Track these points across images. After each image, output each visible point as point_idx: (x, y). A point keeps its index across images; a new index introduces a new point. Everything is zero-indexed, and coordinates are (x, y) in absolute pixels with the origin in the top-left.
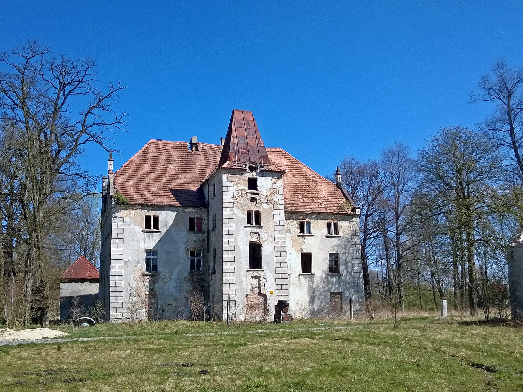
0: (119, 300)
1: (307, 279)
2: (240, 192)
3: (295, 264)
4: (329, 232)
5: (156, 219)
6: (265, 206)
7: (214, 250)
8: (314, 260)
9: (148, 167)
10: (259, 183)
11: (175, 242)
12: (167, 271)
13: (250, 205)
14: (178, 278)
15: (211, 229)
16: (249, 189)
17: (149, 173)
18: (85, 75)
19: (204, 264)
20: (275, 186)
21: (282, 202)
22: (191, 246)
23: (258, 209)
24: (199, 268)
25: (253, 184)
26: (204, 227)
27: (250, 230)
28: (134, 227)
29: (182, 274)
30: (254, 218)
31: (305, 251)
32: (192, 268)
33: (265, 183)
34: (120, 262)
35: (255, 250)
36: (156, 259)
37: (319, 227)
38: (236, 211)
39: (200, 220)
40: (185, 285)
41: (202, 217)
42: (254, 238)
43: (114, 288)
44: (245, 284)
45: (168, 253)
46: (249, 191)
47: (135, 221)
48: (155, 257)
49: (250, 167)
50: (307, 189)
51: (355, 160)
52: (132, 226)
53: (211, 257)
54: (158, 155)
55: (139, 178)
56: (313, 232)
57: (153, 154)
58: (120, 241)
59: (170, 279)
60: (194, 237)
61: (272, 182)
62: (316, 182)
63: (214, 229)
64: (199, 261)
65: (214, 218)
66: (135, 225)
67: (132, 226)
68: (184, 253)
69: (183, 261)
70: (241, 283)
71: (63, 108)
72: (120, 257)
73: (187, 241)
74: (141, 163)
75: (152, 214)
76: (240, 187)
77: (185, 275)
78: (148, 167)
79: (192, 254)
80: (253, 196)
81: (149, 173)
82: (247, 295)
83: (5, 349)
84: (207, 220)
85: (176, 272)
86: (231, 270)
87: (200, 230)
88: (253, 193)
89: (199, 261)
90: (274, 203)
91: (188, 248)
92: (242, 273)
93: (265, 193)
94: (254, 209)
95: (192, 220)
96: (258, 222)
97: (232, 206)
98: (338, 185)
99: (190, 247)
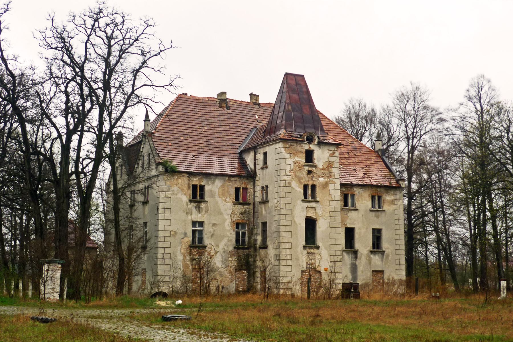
0: (288, 229)
1: (350, 256)
2: (297, 164)
4: (373, 206)
6: (321, 179)
7: (265, 224)
8: (357, 236)
9: (183, 129)
10: (315, 155)
11: (221, 214)
12: (213, 244)
13: (307, 178)
14: (224, 252)
15: (258, 199)
16: (306, 162)
18: (142, 33)
19: (250, 238)
20: (332, 159)
22: (236, 218)
23: (315, 183)
24: (243, 241)
25: (309, 155)
27: (306, 204)
28: (181, 197)
29: (228, 247)
31: (349, 226)
32: (237, 241)
33: (321, 156)
34: (168, 234)
35: (311, 224)
36: (202, 231)
37: (363, 201)
38: (294, 184)
40: (230, 259)
41: (248, 187)
42: (311, 214)
43: (161, 261)
44: (301, 260)
45: (214, 225)
46: (306, 164)
47: (182, 190)
48: (201, 229)
49: (307, 139)
50: (347, 156)
52: (179, 195)
56: (358, 205)
58: (168, 211)
59: (216, 252)
60: (240, 209)
61: (328, 155)
64: (244, 234)
66: (182, 195)
67: (179, 195)
68: (230, 225)
69: (228, 234)
70: (297, 259)
71: (119, 68)
72: (168, 228)
73: (233, 213)
75: (195, 181)
76: (298, 159)
77: (231, 248)
79: (237, 225)
80: (310, 169)
82: (302, 271)
84: (252, 191)
85: (222, 246)
86: (288, 246)
87: (245, 203)
88: (310, 166)
90: (330, 177)
91: (234, 220)
92: (299, 250)
93: (321, 167)
94: (310, 183)
95: (237, 190)
96: (313, 196)
97: (289, 179)
99: (235, 218)
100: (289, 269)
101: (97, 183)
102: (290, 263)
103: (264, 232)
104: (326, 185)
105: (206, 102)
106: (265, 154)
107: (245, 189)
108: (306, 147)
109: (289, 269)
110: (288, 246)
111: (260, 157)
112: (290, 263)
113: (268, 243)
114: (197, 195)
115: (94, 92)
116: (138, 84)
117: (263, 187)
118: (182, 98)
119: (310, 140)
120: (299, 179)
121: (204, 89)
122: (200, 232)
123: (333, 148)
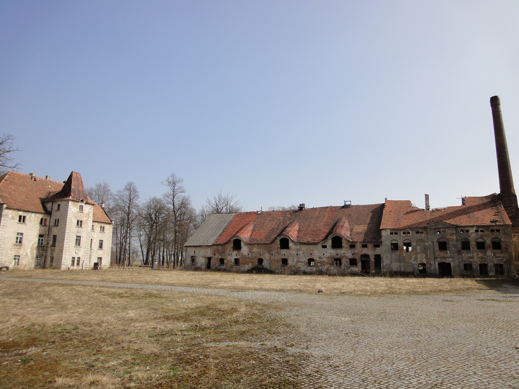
3: (96, 244)
4: (101, 231)
7: (55, 237)
17: (14, 191)
20: (90, 210)
21: (92, 218)
24: (42, 243)
25: (81, 208)
26: (48, 224)
30: (79, 223)
32: (39, 243)
39: (46, 219)
51: (7, 155)
54: (16, 180)
58: (5, 227)
60: (43, 228)
64: (42, 240)
83: (518, 293)
85: (31, 245)
86: (67, 246)
87: (45, 225)
89: (42, 240)
96: (81, 225)
100: (67, 256)
101: (172, 264)
102: (67, 253)
104: (87, 220)
106: (59, 205)
107: (46, 219)
108: (80, 204)
109: (67, 256)
111: (55, 206)
112: (67, 253)
113: (56, 244)
117: (56, 220)
119: (82, 201)
120: (76, 217)
123: (91, 206)
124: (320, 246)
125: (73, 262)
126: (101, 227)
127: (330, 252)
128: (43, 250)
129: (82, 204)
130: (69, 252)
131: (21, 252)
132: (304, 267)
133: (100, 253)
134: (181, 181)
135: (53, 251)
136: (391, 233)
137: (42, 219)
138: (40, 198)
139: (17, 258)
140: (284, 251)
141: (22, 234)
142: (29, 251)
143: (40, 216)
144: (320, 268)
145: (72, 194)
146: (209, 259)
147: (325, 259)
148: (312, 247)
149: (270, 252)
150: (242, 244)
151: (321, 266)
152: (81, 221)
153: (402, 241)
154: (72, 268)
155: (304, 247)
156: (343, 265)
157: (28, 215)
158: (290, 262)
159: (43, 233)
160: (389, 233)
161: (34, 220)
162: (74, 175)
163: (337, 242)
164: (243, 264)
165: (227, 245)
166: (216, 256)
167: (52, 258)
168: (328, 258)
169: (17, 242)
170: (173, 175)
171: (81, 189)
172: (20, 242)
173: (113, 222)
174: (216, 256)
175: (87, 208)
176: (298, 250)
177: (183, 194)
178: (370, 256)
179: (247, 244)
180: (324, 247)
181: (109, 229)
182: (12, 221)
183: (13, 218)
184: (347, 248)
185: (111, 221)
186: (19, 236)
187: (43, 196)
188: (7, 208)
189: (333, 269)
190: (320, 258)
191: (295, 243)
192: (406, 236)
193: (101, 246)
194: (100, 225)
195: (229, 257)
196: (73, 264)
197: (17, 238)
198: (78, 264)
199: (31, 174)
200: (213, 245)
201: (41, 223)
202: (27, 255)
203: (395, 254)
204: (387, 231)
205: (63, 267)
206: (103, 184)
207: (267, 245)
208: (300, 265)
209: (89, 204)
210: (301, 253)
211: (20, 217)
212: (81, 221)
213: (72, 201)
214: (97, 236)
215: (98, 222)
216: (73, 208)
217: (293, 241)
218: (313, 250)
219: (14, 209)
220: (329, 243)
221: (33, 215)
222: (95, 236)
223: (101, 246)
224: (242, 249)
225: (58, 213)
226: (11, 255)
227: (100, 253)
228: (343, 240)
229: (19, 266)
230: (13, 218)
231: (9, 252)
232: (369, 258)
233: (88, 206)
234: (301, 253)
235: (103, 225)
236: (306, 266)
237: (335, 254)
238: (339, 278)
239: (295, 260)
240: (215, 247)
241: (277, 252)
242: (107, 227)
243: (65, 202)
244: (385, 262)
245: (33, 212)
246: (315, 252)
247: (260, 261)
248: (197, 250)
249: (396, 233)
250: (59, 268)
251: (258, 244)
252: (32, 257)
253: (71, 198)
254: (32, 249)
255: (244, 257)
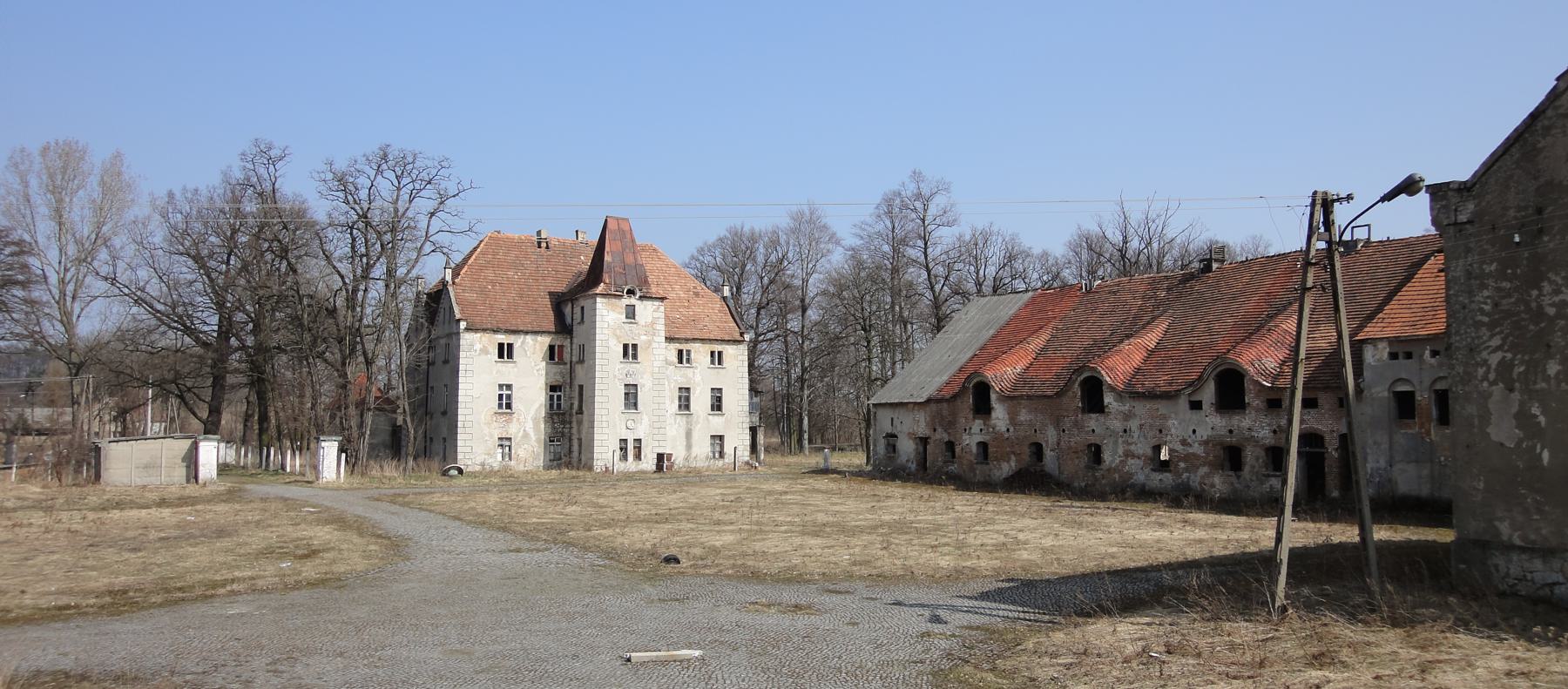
3: (701, 401)
5: (510, 346)
7: (581, 387)
17: (493, 283)
20: (656, 315)
24: (559, 406)
25: (631, 313)
26: (567, 357)
30: (630, 352)
32: (551, 406)
53: (576, 394)
55: (483, 291)
57: (495, 254)
60: (555, 369)
62: (697, 294)
63: (581, 361)
64: (559, 398)
65: (582, 348)
74: (482, 268)
78: (490, 274)
81: (493, 283)
86: (604, 412)
87: (561, 362)
89: (559, 398)
96: (635, 356)
98: (724, 299)
103: (581, 394)
104: (650, 343)
105: (519, 244)
107: (561, 347)
108: (626, 301)
110: (604, 412)
111: (577, 310)
114: (505, 352)
115: (380, 235)
116: (432, 230)
118: (183, 460)
119: (631, 292)
120: (618, 338)
121: (520, 230)
122: (509, 397)
124: (1183, 403)
125: (624, 449)
126: (712, 353)
127: (1212, 423)
128: (563, 422)
129: (633, 301)
130: (609, 427)
131: (513, 430)
132: (1141, 474)
133: (717, 424)
134: (943, 187)
135: (580, 423)
136: (1393, 356)
137: (551, 348)
138: (550, 293)
139: (505, 442)
140: (1093, 421)
141: (509, 387)
142: (529, 426)
143: (545, 341)
144: (1185, 475)
145: (606, 277)
146: (924, 441)
147: (1197, 449)
148: (1162, 407)
149: (1057, 422)
150: (993, 397)
151: (1186, 470)
152: (635, 346)
153: (1427, 383)
154: (620, 467)
155: (1142, 408)
156: (1247, 469)
157: (518, 341)
158: (1107, 456)
159: (558, 380)
160: (1386, 355)
161: (531, 350)
162: (612, 225)
163: (1231, 388)
164: (997, 459)
165: (959, 402)
166: (938, 436)
167: (580, 440)
168: (1206, 443)
169: (500, 406)
170: (917, 176)
171: (630, 259)
172: (509, 406)
173: (747, 337)
174: (938, 436)
175: (647, 311)
176: (1127, 416)
177: (955, 230)
178: (1327, 438)
179: (1005, 398)
180: (1196, 406)
181: (737, 357)
182: (483, 357)
183: (484, 351)
184: (1257, 410)
185: (742, 334)
186: (505, 392)
187: (561, 288)
188: (467, 329)
189: (1219, 483)
190: (1184, 442)
191: (1120, 396)
192: (1441, 365)
193: (717, 405)
194: (708, 348)
195: (965, 437)
196: (624, 457)
197: (501, 396)
198: (638, 456)
199: (539, 233)
200: (929, 401)
201: (552, 357)
202: (526, 435)
203: (1405, 435)
204: (1381, 345)
205: (598, 465)
206: (806, 208)
207: (1048, 402)
208: (1133, 465)
209: (651, 298)
210: (1134, 424)
211: (501, 346)
212: (635, 346)
213: (603, 295)
214: (701, 377)
215: (703, 340)
216: (607, 316)
217: (1112, 389)
218: (1165, 418)
219: (484, 330)
220: (1208, 394)
221: (529, 338)
222: (698, 378)
223: (717, 405)
224: (994, 415)
225: (583, 327)
226: (491, 436)
227: (717, 424)
228: (1248, 385)
229: (513, 463)
230: (484, 351)
231: (486, 431)
232: (1323, 445)
233: (648, 303)
234: (1134, 424)
235: (717, 348)
236: (1147, 470)
237: (1224, 432)
238: (1161, 513)
239: (1120, 451)
240: (933, 406)
241: (1076, 424)
242: (729, 351)
243: (590, 301)
244: (1372, 461)
245: (527, 333)
246: (1170, 422)
247: (1038, 450)
248: (898, 415)
249: (1409, 356)
250: (590, 468)
251: (1029, 397)
252: (538, 441)
253: (601, 288)
254: (535, 420)
255: (998, 437)
